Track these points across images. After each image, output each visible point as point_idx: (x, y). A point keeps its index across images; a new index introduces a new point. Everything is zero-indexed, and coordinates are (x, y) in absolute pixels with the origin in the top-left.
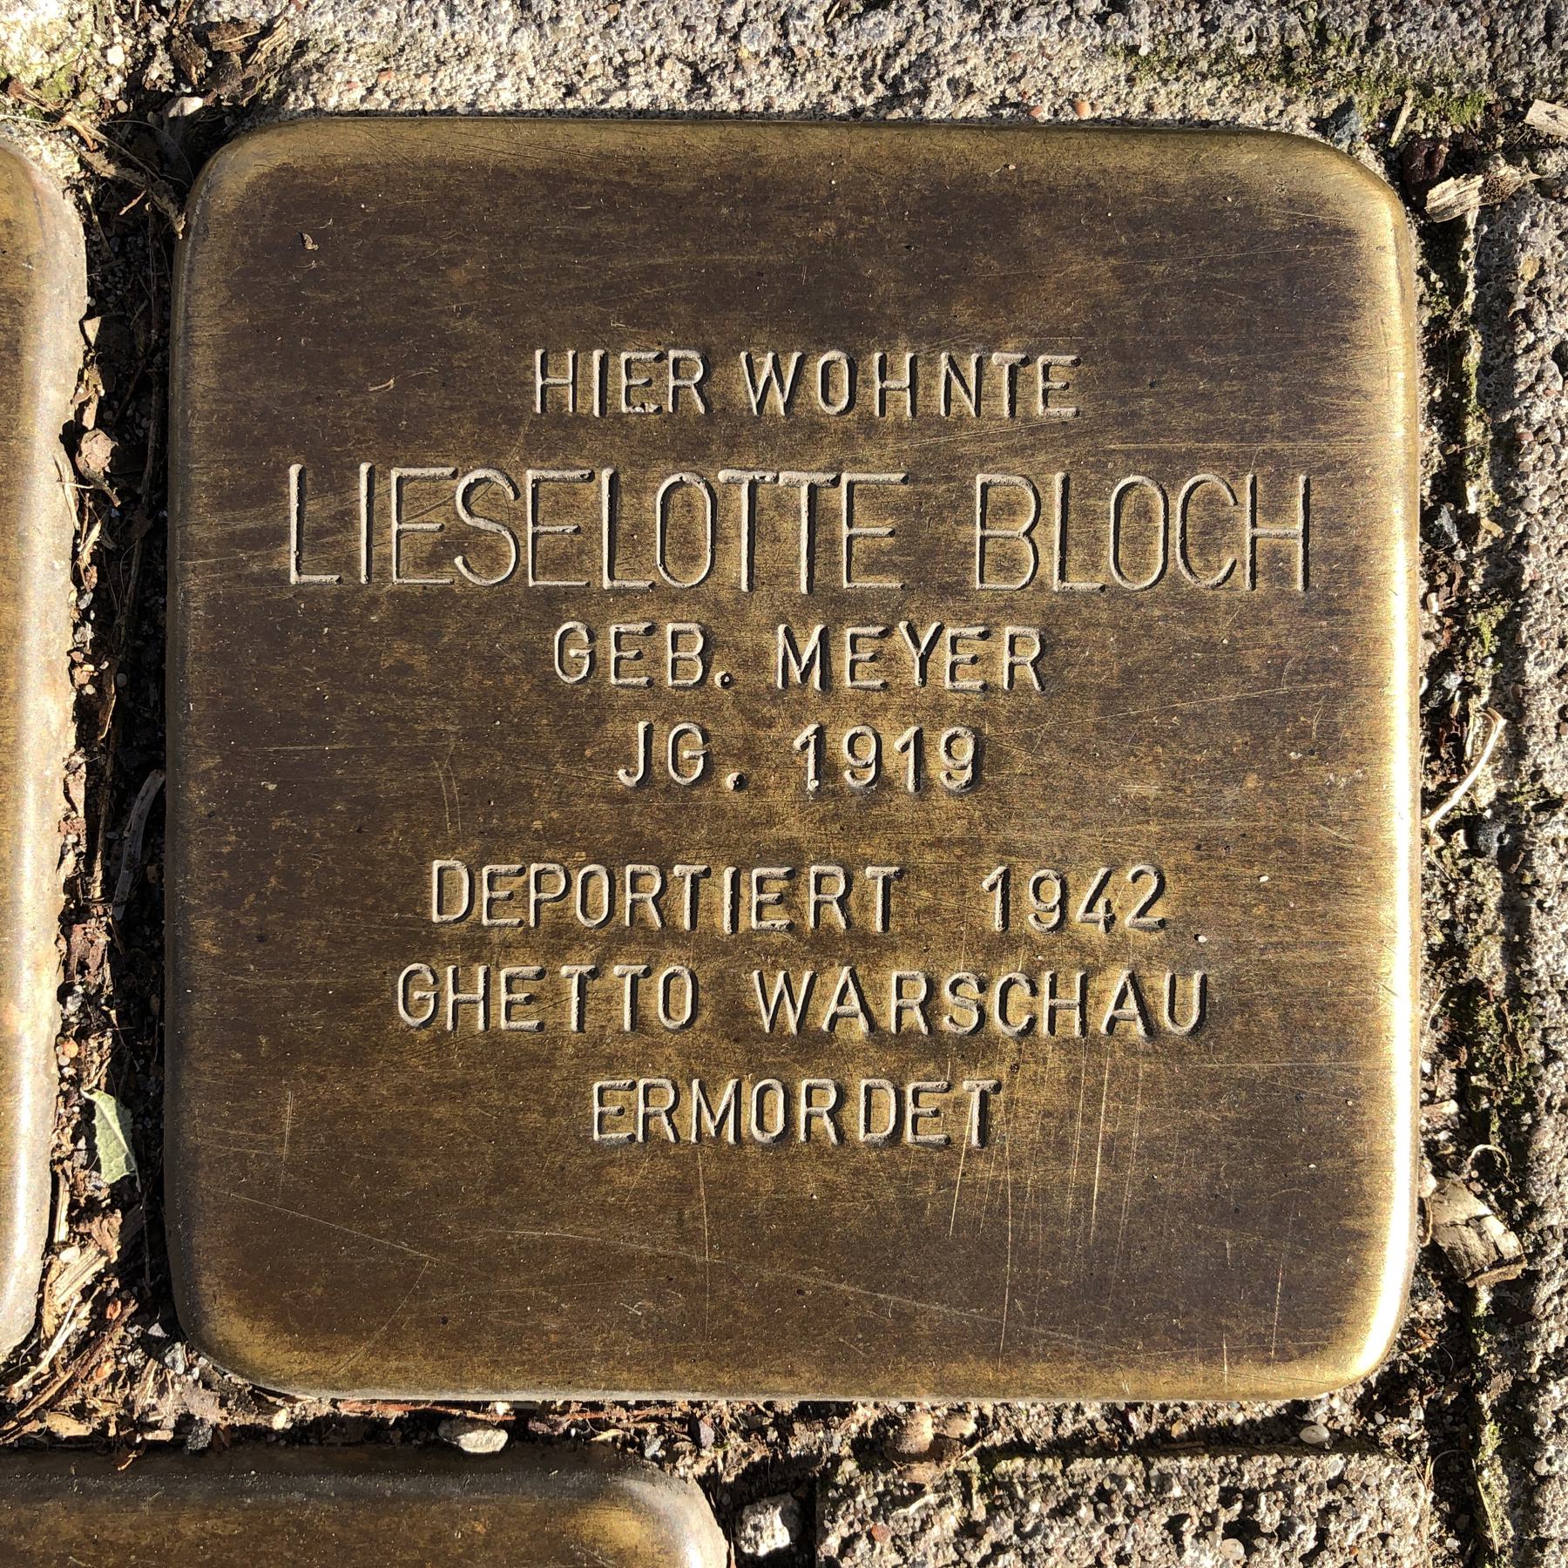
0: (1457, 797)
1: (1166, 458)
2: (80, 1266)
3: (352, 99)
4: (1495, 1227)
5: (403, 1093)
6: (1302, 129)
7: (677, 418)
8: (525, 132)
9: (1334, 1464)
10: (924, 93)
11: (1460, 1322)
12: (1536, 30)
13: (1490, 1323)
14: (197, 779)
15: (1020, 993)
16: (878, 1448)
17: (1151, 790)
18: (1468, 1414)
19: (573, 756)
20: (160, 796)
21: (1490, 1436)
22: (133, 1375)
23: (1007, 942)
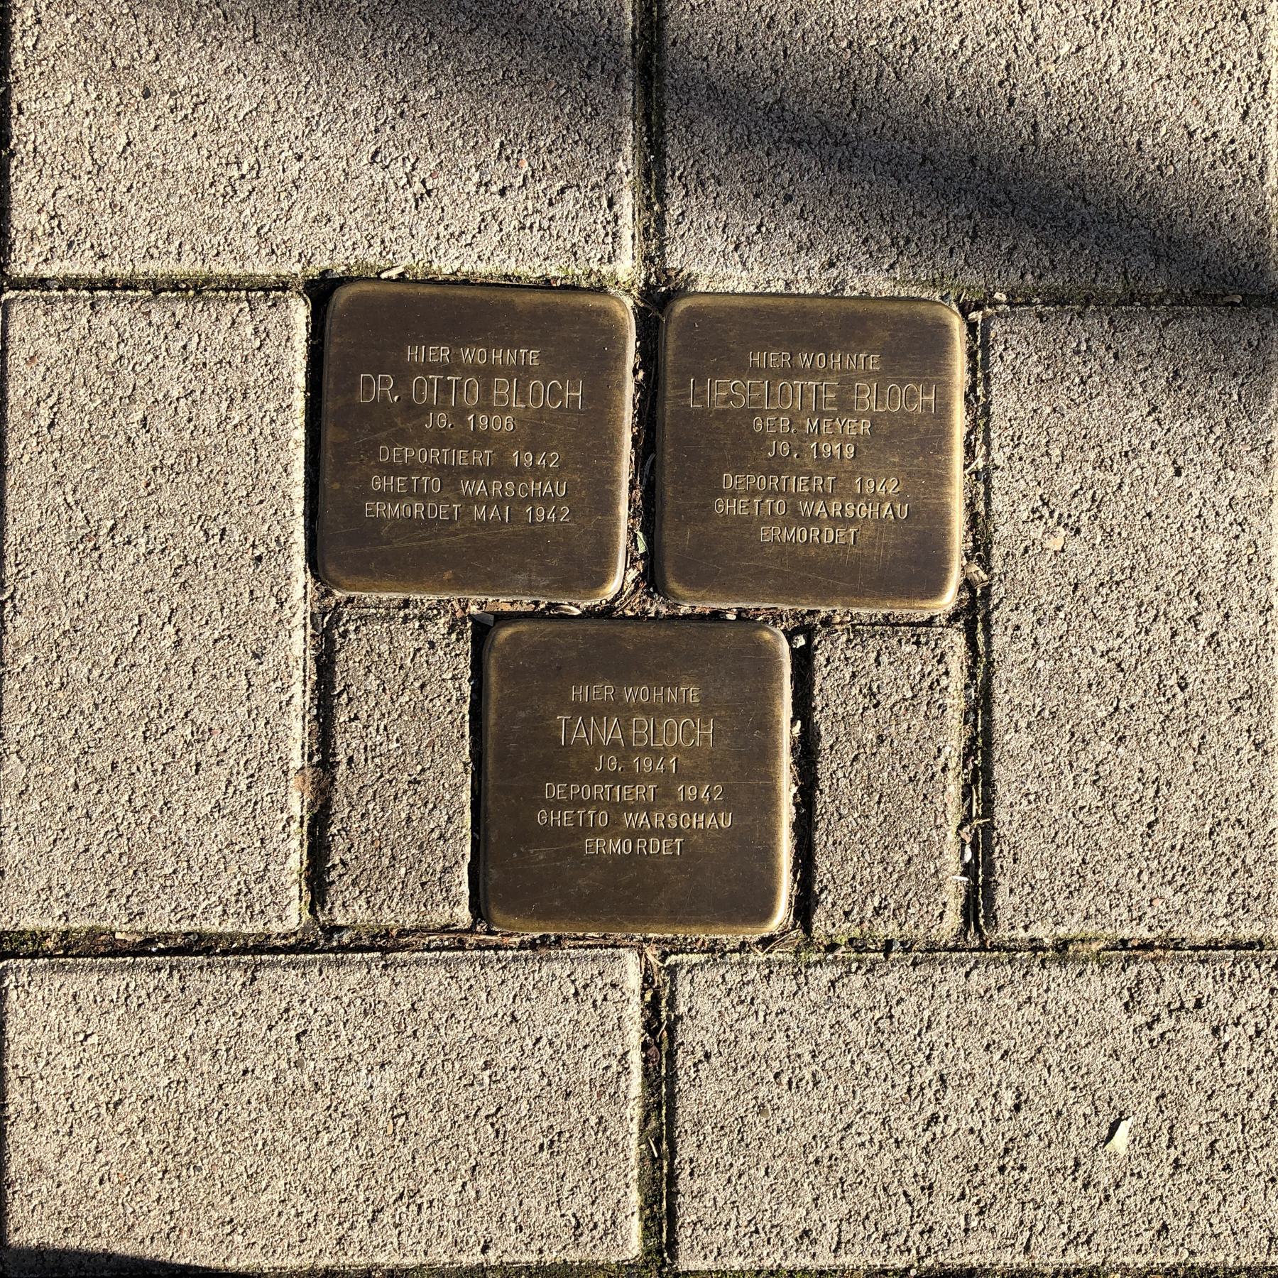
0: (973, 466)
1: (901, 380)
2: (633, 574)
3: (703, 289)
4: (981, 573)
5: (716, 529)
6: (937, 299)
7: (784, 369)
8: (748, 299)
9: (940, 630)
10: (843, 290)
11: (973, 599)
12: (996, 275)
13: (980, 598)
14: (668, 453)
15: (864, 508)
16: (827, 622)
17: (896, 460)
18: (975, 621)
19: (758, 449)
20: (654, 461)
21: (980, 626)
22: (644, 601)
23: (861, 495)
